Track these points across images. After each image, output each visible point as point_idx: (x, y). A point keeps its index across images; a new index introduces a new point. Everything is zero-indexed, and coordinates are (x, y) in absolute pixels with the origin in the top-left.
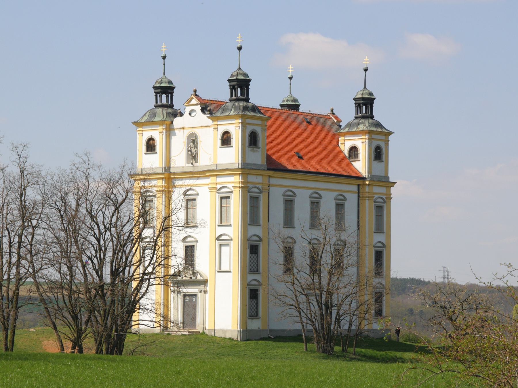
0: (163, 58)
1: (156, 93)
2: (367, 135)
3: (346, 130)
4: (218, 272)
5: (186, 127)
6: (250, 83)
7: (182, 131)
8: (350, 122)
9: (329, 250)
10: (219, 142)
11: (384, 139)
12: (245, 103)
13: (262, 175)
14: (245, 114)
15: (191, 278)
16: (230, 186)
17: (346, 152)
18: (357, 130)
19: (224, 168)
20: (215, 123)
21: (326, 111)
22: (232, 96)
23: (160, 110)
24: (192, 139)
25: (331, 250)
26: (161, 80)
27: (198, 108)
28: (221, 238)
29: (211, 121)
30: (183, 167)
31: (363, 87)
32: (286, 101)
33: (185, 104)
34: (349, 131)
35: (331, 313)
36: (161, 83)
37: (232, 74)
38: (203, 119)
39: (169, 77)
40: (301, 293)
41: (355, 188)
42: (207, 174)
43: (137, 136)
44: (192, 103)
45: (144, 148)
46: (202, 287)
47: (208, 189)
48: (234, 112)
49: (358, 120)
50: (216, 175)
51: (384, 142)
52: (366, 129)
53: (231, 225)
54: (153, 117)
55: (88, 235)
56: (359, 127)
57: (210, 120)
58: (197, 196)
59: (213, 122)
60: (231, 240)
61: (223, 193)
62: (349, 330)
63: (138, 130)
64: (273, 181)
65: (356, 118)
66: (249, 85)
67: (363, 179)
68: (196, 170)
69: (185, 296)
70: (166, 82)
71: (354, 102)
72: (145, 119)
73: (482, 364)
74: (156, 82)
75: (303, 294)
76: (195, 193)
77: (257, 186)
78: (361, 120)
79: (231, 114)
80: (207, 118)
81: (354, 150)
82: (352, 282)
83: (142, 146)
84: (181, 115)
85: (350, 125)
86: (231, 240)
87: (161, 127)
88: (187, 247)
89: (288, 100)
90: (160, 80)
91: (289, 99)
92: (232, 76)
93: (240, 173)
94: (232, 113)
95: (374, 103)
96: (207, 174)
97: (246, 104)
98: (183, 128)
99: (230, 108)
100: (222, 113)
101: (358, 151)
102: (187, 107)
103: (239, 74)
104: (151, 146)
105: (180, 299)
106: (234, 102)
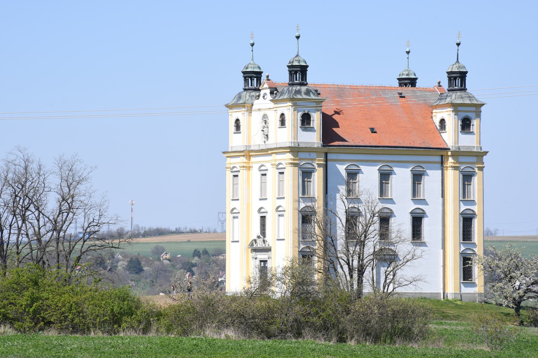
0: (251, 45)
1: (245, 77)
2: (451, 107)
4: (278, 240)
7: (259, 112)
9: (93, 228)
11: (475, 110)
13: (316, 152)
16: (237, 166)
17: (437, 124)
20: (276, 106)
29: (273, 104)
30: (259, 145)
31: (456, 60)
36: (247, 68)
39: (258, 62)
41: (438, 159)
42: (270, 152)
47: (271, 165)
50: (276, 153)
53: (284, 198)
58: (267, 171)
69: (261, 261)
70: (251, 68)
71: (288, 69)
73: (63, 309)
77: (310, 162)
79: (284, 98)
83: (232, 127)
87: (243, 109)
88: (261, 217)
89: (403, 74)
92: (290, 63)
96: (270, 152)
98: (259, 110)
103: (294, 61)
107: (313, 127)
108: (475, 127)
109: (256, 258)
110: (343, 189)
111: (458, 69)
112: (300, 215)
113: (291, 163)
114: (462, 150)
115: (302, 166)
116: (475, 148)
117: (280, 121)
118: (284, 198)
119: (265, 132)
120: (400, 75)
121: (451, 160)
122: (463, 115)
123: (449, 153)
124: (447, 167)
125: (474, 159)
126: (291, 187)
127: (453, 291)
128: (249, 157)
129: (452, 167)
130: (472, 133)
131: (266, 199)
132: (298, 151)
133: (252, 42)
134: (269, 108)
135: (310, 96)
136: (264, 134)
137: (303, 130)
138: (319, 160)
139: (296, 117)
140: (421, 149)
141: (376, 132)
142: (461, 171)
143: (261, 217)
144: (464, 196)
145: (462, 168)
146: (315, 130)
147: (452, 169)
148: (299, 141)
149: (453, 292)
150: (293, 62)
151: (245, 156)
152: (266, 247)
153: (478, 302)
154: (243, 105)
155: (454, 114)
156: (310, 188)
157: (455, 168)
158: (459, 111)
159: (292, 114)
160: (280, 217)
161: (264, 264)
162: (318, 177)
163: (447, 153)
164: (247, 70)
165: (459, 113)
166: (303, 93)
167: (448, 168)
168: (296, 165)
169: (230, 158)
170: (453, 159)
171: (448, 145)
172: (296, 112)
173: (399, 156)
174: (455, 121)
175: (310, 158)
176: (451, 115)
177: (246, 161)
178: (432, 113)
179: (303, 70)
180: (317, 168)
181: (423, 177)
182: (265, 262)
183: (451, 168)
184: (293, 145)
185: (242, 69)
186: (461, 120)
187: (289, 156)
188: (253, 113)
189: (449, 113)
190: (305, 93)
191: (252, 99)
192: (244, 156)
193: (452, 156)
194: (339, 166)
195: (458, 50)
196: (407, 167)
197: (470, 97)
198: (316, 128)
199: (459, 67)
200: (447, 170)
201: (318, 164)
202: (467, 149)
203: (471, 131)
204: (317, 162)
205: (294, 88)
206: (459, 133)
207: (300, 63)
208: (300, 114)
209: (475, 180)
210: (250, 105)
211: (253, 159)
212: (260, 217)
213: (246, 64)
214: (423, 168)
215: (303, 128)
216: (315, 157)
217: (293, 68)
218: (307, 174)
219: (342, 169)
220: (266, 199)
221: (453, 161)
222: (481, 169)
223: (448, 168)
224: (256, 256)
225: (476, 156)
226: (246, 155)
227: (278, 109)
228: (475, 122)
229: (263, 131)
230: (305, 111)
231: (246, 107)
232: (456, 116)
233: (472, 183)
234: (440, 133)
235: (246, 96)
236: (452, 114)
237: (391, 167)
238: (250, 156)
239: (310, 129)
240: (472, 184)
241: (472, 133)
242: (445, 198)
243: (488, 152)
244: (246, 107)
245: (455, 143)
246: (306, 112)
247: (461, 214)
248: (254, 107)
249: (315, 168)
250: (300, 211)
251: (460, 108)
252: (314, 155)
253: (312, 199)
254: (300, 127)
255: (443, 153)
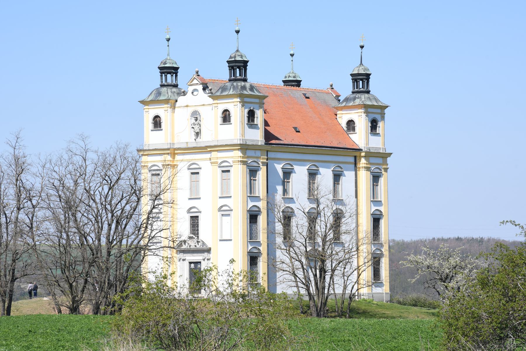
0: (167, 40)
1: (162, 73)
2: (363, 109)
3: (344, 104)
4: (220, 240)
5: (189, 105)
6: (248, 64)
7: (186, 108)
8: (347, 97)
10: (220, 120)
11: (380, 112)
12: (243, 83)
14: (243, 94)
15: (196, 246)
17: (344, 125)
18: (354, 104)
19: (224, 144)
20: (216, 101)
21: (326, 87)
22: (231, 76)
23: (164, 89)
24: (195, 116)
25: (325, 219)
26: (166, 61)
27: (200, 87)
28: (222, 209)
30: (187, 143)
32: (288, 77)
33: (188, 84)
34: (346, 105)
35: (324, 278)
36: (165, 63)
37: (231, 56)
38: (203, 97)
40: (296, 259)
41: (352, 160)
42: (209, 150)
43: (144, 113)
44: (193, 83)
45: (151, 126)
46: (206, 254)
48: (233, 91)
49: (354, 95)
50: (217, 151)
51: (380, 115)
52: (362, 103)
53: (231, 196)
54: (158, 96)
55: (83, 215)
56: (355, 101)
57: (211, 99)
59: (213, 101)
60: (232, 210)
61: (223, 167)
62: (344, 294)
63: (144, 108)
64: (271, 155)
65: (353, 93)
66: (247, 66)
67: (360, 150)
68: (199, 145)
69: (190, 263)
70: (170, 63)
71: (351, 77)
72: (151, 98)
74: (162, 62)
75: (297, 260)
76: (197, 167)
78: (358, 95)
79: (229, 94)
80: (208, 97)
81: (351, 124)
82: (257, 318)
84: (184, 93)
85: (347, 100)
86: (232, 210)
87: (166, 106)
89: (289, 76)
90: (164, 61)
91: (291, 75)
92: (231, 57)
93: (239, 149)
94: (231, 92)
95: (370, 78)
97: (244, 84)
98: (187, 106)
99: (229, 88)
100: (222, 92)
101: (355, 124)
102: (190, 87)
103: (237, 56)
104: (157, 123)
105: (186, 265)
106: (232, 82)
107: (257, 125)
108: (381, 128)
109: (184, 260)
110: (280, 188)
111: (364, 71)
112: (248, 214)
113: (241, 161)
114: (371, 151)
115: (250, 164)
116: (381, 150)
117: (222, 117)
118: (231, 196)
119: (195, 129)
120: (286, 77)
121: (363, 161)
122: (373, 116)
123: (363, 154)
124: (360, 168)
125: (380, 161)
126: (240, 185)
127: (367, 291)
128: (173, 155)
129: (365, 168)
130: (378, 134)
131: (200, 198)
132: (247, 149)
133: (168, 37)
134: (202, 104)
135: (253, 92)
136: (194, 132)
137: (249, 128)
138: (263, 158)
139: (243, 113)
140: (341, 150)
141: (299, 132)
142: (372, 172)
143: (191, 217)
144: (251, 193)
145: (373, 169)
146: (258, 127)
147: (365, 170)
148: (246, 138)
149: (367, 292)
150: (235, 57)
151: (170, 154)
152: (201, 248)
153: (386, 301)
154: (167, 101)
155: (366, 116)
156: (256, 186)
157: (368, 169)
158: (369, 112)
159: (240, 110)
160: (223, 217)
161: (196, 266)
162: (261, 175)
163: (360, 153)
164: (166, 66)
165: (369, 115)
166: (248, 90)
167: (360, 168)
168: (245, 163)
169: (147, 156)
170: (366, 160)
171: (360, 146)
172: (243, 108)
173: (339, 156)
174: (366, 122)
175: (255, 156)
176: (363, 116)
177: (171, 159)
178: (336, 115)
179: (243, 65)
180: (261, 166)
181: (341, 177)
182: (197, 263)
183: (364, 169)
184: (241, 143)
185: (159, 64)
186: (370, 122)
187: (239, 154)
188: (176, 109)
189: (360, 114)
190: (249, 89)
191: (174, 96)
192: (168, 154)
193: (365, 157)
194: (276, 165)
195: (362, 53)
196: (329, 168)
197: (376, 100)
198: (259, 126)
199: (365, 69)
200: (359, 170)
201: (262, 163)
202: (375, 150)
203: (378, 132)
204: (261, 161)
205: (239, 84)
206: (369, 134)
207: (243, 59)
208: (247, 111)
209: (382, 180)
210: (173, 102)
211: (177, 157)
212: (190, 217)
213: (163, 59)
214: (341, 168)
215: (249, 125)
216: (260, 155)
217: (236, 63)
218: (253, 172)
219: (279, 167)
220: (200, 198)
221: (365, 162)
222: (386, 170)
223: (361, 169)
224: (184, 258)
225: (382, 157)
226: (171, 153)
227: (219, 105)
228: (380, 124)
229: (193, 128)
230: (250, 108)
231: (170, 104)
232: (367, 118)
233: (379, 184)
234: (348, 134)
235: (167, 93)
236: (364, 115)
237: (317, 167)
238: (175, 154)
239: (255, 126)
240: (291, 182)
241: (378, 134)
242: (358, 199)
243: (392, 154)
244: (170, 104)
245: (366, 144)
246: (252, 109)
247: (248, 211)
248: (178, 104)
249: (260, 166)
250: (248, 211)
251: (370, 110)
252: (258, 153)
253: (258, 198)
254: (247, 124)
255: (357, 154)
